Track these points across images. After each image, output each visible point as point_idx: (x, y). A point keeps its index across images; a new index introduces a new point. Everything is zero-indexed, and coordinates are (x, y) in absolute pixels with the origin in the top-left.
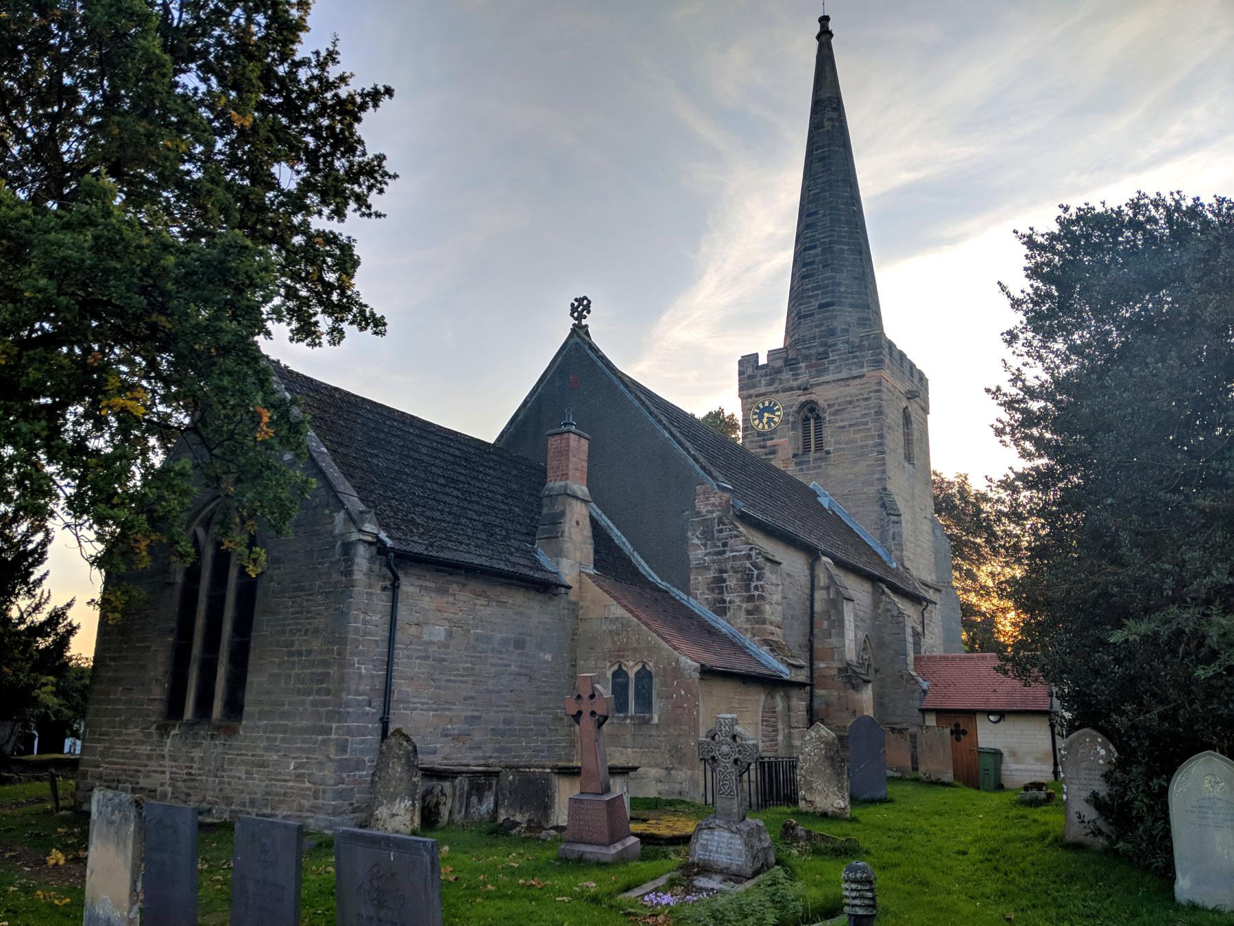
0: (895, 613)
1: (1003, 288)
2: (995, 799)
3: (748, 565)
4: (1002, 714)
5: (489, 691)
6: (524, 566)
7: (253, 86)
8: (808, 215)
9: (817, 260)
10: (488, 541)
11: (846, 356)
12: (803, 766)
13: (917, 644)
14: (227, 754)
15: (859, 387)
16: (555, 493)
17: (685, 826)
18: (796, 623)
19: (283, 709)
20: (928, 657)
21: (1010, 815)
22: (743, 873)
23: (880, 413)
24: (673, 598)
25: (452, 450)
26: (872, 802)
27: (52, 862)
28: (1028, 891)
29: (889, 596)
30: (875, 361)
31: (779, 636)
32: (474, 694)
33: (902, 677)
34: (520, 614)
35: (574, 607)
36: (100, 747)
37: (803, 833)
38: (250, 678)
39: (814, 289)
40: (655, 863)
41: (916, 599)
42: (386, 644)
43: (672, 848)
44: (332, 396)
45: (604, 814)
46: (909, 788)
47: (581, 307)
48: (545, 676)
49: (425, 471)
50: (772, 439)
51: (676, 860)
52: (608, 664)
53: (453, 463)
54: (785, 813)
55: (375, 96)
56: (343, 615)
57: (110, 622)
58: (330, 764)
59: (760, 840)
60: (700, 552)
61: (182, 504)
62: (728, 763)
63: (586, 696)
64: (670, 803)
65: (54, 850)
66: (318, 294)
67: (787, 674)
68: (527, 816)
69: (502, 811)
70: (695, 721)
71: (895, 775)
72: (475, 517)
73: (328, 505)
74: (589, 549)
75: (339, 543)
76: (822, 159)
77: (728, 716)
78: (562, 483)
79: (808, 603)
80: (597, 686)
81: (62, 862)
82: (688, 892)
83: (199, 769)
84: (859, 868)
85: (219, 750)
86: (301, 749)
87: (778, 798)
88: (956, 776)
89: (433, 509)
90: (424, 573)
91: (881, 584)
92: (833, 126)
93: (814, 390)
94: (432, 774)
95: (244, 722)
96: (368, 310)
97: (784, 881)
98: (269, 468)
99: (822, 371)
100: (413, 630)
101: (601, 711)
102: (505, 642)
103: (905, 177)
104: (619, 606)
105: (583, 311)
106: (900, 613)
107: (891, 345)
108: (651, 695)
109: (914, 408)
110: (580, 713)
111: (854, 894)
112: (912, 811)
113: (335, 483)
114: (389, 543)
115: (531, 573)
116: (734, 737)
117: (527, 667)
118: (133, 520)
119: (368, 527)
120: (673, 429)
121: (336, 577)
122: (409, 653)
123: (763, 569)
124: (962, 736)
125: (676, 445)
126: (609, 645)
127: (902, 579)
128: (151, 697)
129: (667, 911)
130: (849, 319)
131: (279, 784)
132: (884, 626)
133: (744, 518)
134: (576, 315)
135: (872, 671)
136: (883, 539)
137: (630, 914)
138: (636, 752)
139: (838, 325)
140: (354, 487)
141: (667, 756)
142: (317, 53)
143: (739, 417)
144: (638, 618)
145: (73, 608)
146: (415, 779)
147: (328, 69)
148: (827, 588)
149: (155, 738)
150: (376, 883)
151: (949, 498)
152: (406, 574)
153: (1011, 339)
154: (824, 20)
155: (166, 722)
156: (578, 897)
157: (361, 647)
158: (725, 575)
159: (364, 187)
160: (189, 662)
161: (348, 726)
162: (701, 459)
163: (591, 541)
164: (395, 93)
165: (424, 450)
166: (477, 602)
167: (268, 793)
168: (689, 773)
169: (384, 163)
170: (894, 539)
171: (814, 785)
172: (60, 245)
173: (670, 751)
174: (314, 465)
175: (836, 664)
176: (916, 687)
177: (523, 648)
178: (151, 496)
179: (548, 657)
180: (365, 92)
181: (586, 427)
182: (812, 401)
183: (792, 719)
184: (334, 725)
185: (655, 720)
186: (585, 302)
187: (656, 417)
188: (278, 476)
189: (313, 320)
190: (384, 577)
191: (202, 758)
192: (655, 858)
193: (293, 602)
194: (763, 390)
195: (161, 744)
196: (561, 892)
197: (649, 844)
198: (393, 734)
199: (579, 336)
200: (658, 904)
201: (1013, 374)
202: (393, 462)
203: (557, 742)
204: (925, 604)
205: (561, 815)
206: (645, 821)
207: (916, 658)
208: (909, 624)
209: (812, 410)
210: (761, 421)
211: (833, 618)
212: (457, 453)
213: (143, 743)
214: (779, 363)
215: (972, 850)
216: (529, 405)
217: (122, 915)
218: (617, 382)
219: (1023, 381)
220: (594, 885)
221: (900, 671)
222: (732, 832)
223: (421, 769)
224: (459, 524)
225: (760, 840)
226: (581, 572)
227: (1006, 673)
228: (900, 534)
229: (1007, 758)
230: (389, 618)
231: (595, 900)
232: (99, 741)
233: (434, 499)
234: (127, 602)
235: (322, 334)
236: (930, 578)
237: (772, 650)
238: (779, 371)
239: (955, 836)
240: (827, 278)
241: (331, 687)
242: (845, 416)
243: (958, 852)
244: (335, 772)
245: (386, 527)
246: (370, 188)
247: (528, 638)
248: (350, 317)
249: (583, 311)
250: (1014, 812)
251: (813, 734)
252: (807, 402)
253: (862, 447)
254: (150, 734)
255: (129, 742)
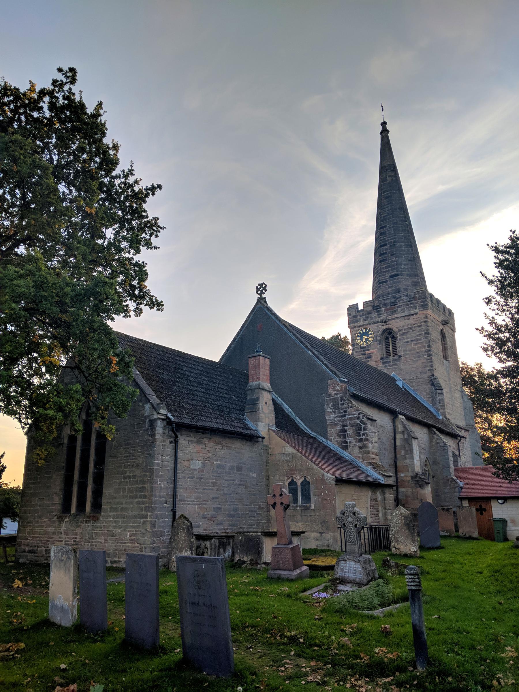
0: (442, 444)
1: (483, 275)
2: (501, 546)
3: (359, 422)
4: (505, 499)
5: (225, 494)
6: (240, 428)
7: (95, 193)
8: (381, 228)
9: (387, 252)
10: (221, 415)
11: (406, 303)
12: (393, 530)
13: (456, 462)
14: (94, 530)
15: (415, 319)
16: (253, 388)
17: (331, 561)
18: (386, 453)
19: (122, 506)
20: (462, 468)
21: (508, 553)
22: (362, 582)
23: (427, 333)
24: (318, 441)
25: (199, 368)
26: (432, 548)
27: (16, 586)
28: (513, 590)
29: (438, 436)
30: (423, 305)
31: (377, 460)
32: (217, 496)
33: (448, 480)
34: (238, 453)
35: (266, 448)
36: (28, 529)
37: (393, 564)
38: (104, 491)
39: (386, 267)
40: (318, 579)
41: (453, 436)
42: (173, 471)
43: (325, 572)
44: (139, 344)
45: (290, 554)
46: (453, 541)
47: (261, 289)
48: (254, 485)
49: (187, 380)
50: (369, 350)
51: (327, 578)
52: (286, 478)
53: (200, 375)
54: (384, 555)
55: (153, 189)
56: (150, 457)
57: (39, 465)
58: (148, 533)
59: (370, 566)
60: (332, 416)
61: (77, 406)
62: (352, 526)
63: (278, 495)
64: (323, 551)
65: (16, 580)
66: (127, 292)
67: (382, 480)
68: (250, 557)
69: (237, 555)
70: (334, 507)
71: (446, 534)
72: (213, 402)
73: (141, 401)
74: (272, 416)
75: (148, 419)
76: (387, 197)
77: (351, 503)
78: (257, 382)
79: (393, 441)
80: (283, 489)
81: (21, 586)
82: (334, 591)
83: (80, 539)
84: (413, 568)
85: (90, 528)
86: (132, 526)
87: (381, 548)
88: (480, 534)
89: (192, 400)
90: (190, 433)
91: (433, 429)
92: (392, 180)
93: (390, 322)
94: (200, 537)
95: (102, 514)
96: (154, 298)
97: (382, 584)
98: (116, 385)
99: (393, 313)
100: (186, 463)
101: (286, 501)
102: (232, 468)
103: (441, 188)
104: (290, 447)
105: (263, 290)
106: (445, 444)
107: (431, 296)
108: (309, 494)
109: (446, 329)
110: (275, 503)
111: (410, 580)
112: (454, 553)
113: (144, 389)
114: (173, 419)
115: (244, 431)
116: (354, 514)
117: (244, 481)
118: (56, 415)
119: (162, 411)
120: (314, 351)
121: (147, 437)
122: (184, 475)
123: (366, 424)
124: (483, 512)
125: (316, 359)
126: (286, 468)
127: (446, 425)
128: (54, 502)
129: (324, 601)
130: (407, 283)
131: (121, 544)
132: (436, 452)
133: (355, 397)
134: (259, 292)
135: (431, 478)
136: (433, 403)
137: (306, 602)
138: (303, 524)
139: (402, 286)
140: (153, 390)
141: (320, 526)
142: (123, 171)
143: (349, 338)
144: (301, 453)
145: (4, 457)
146: (192, 540)
147: (129, 179)
148: (403, 432)
149: (57, 523)
150: (196, 579)
151: (472, 377)
152: (181, 435)
153: (489, 301)
154: (384, 124)
155: (62, 515)
156: (281, 594)
157: (161, 473)
158: (346, 428)
159: (148, 234)
160: (72, 484)
161: (156, 514)
162: (330, 366)
163: (274, 412)
164: (163, 187)
165: (185, 369)
166: (217, 447)
167: (116, 550)
168: (332, 534)
169: (158, 221)
170: (440, 403)
171: (399, 539)
172: (19, 286)
173: (321, 523)
174: (136, 385)
175: (410, 474)
176: (456, 485)
177: (241, 471)
178: (64, 403)
179: (254, 475)
180: (148, 188)
181: (269, 353)
182: (389, 329)
183: (386, 505)
184: (149, 514)
185: (313, 507)
186: (264, 286)
187: (304, 344)
188: (121, 389)
189: (125, 304)
190: (170, 437)
191: (81, 533)
192: (317, 577)
193: (126, 451)
194: (362, 323)
195: (60, 526)
196: (271, 593)
197: (313, 570)
198: (180, 517)
199: (261, 303)
200: (319, 598)
201: (490, 320)
202: (171, 376)
203: (261, 520)
204: (459, 438)
205: (267, 556)
206: (310, 560)
207: (455, 469)
208: (450, 450)
209: (390, 333)
210: (362, 341)
211: (407, 449)
212: (202, 369)
213: (50, 526)
214: (370, 309)
215: (485, 571)
216: (236, 340)
217: (69, 604)
218: (283, 327)
219: (495, 323)
220: (287, 589)
221: (447, 477)
222: (356, 562)
223: (195, 535)
224: (205, 407)
225: (370, 566)
226: (269, 429)
227: (498, 476)
228: (443, 400)
229: (509, 524)
230: (174, 457)
231: (289, 596)
232: (27, 526)
233: (192, 394)
234: (47, 454)
235: (131, 311)
236: (462, 424)
237: (374, 468)
238: (370, 313)
239: (477, 564)
240: (394, 261)
241: (146, 494)
242: (408, 336)
243: (478, 573)
244: (151, 538)
245: (170, 411)
246: (151, 235)
247: (243, 466)
248: (145, 302)
249: (263, 290)
250: (511, 552)
251: (397, 512)
252: (387, 329)
253: (419, 353)
254: (54, 522)
255: (43, 526)
